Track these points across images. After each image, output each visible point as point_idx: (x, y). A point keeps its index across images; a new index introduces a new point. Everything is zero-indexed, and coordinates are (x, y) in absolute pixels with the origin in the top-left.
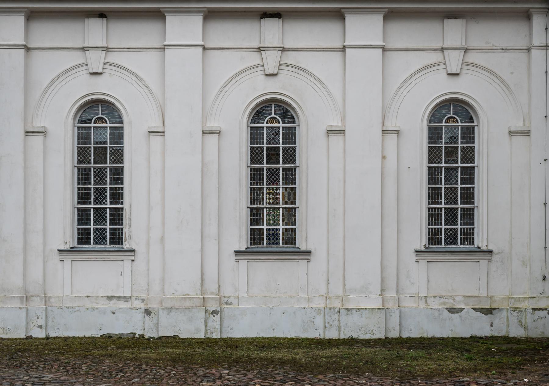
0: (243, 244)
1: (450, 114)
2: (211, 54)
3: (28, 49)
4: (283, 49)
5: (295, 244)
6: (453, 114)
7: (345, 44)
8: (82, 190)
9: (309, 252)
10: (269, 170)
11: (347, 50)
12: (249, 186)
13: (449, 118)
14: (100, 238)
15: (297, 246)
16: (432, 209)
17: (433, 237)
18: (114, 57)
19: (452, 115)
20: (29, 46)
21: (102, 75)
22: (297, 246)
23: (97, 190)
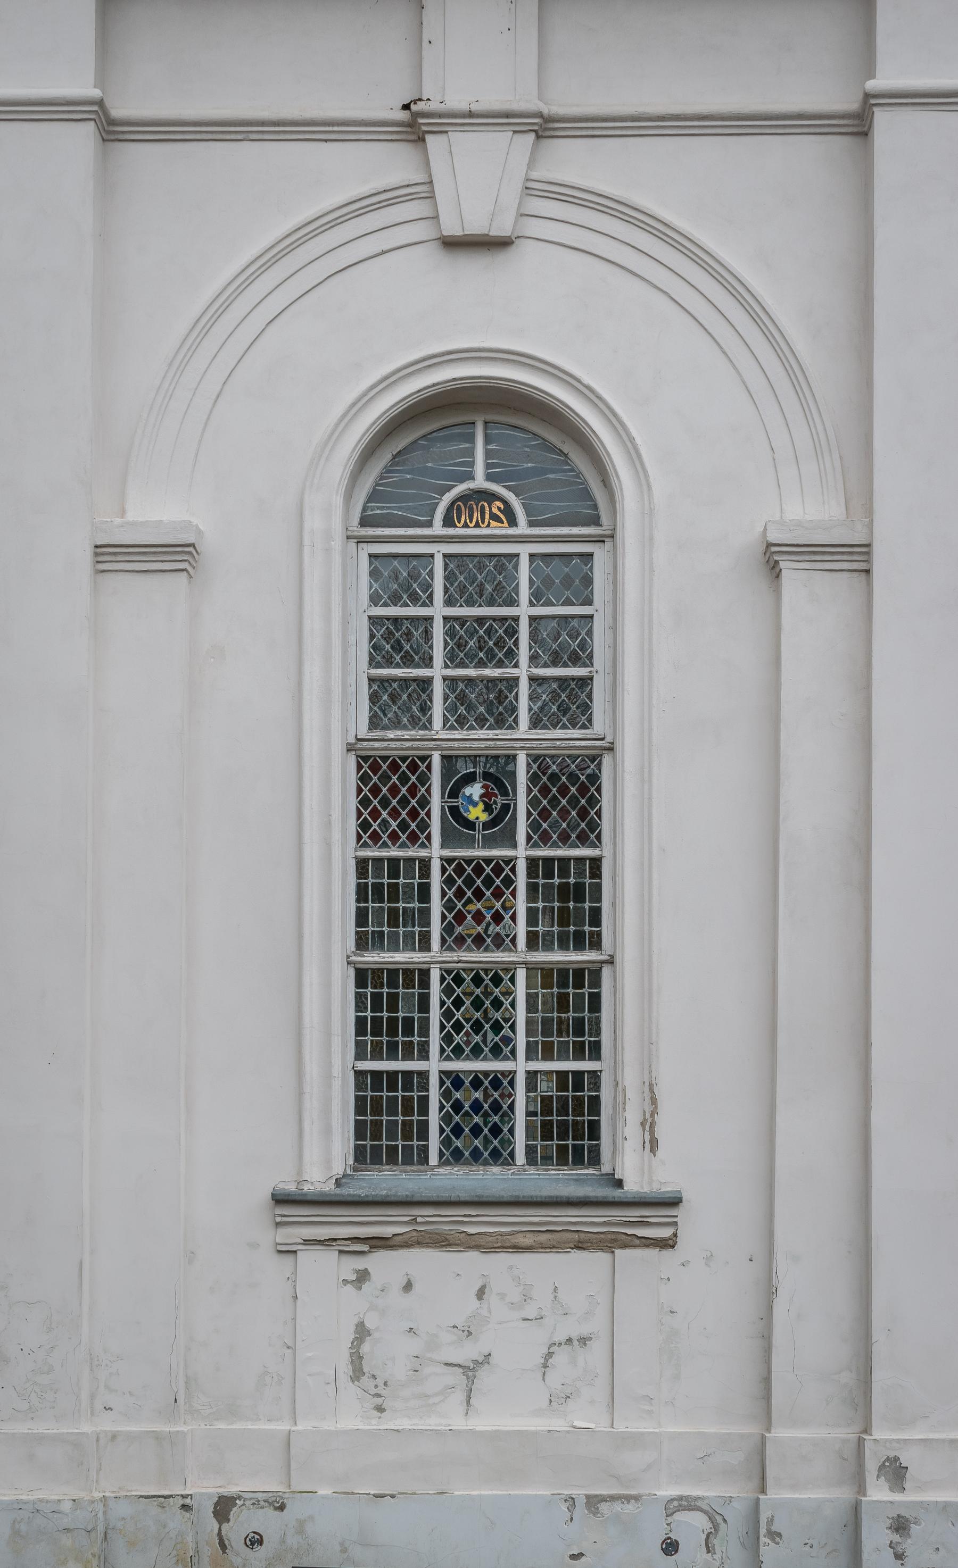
0: (325, 1153)
1: (471, 477)
2: (141, 158)
3: (113, 131)
4: (545, 127)
5: (595, 1160)
6: (489, 477)
7: (872, 85)
8: (378, 874)
9: (674, 1202)
10: (375, 768)
11: (882, 119)
12: (606, 851)
13: (464, 498)
14: (478, 1126)
15: (606, 1168)
16: (377, 973)
18: (571, 162)
19: (480, 481)
20: (117, 112)
21: (512, 252)
22: (606, 1168)
23: (460, 870)
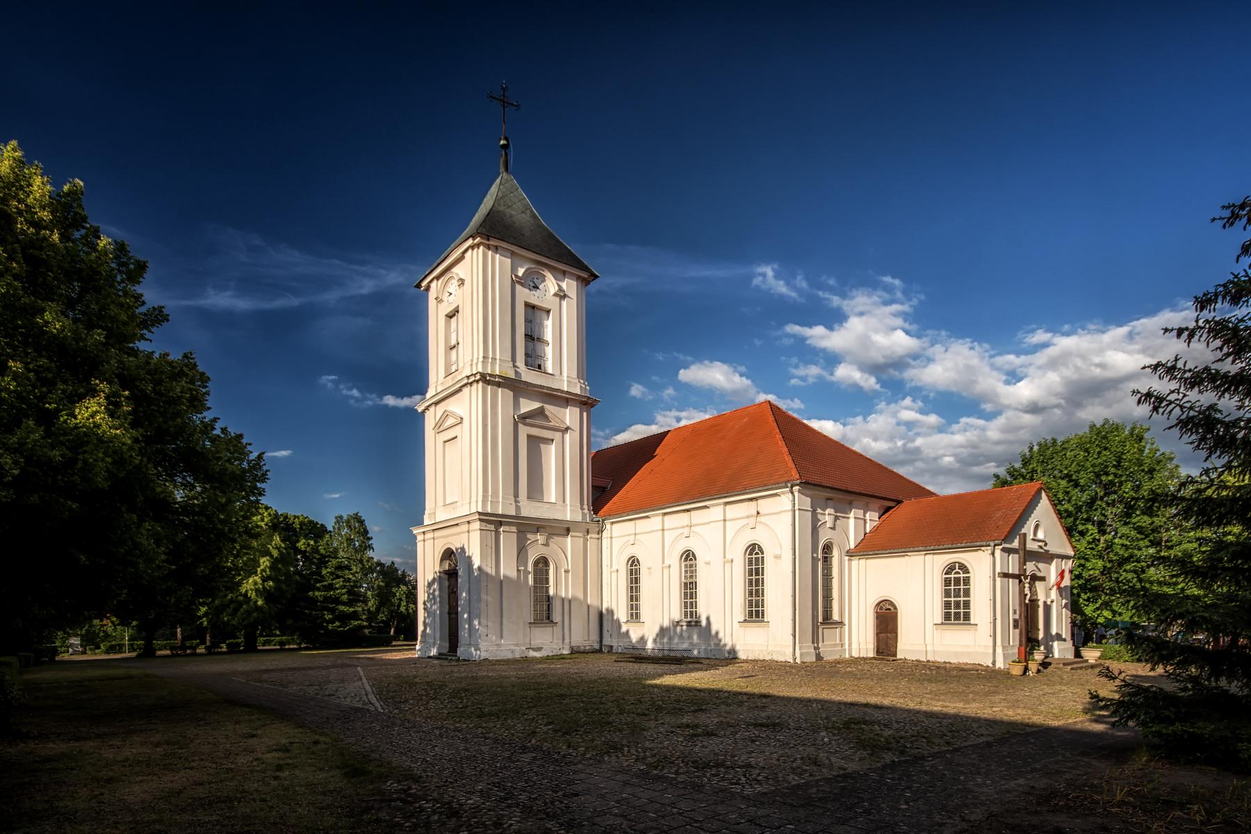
14: (957, 616)
17: (947, 616)
